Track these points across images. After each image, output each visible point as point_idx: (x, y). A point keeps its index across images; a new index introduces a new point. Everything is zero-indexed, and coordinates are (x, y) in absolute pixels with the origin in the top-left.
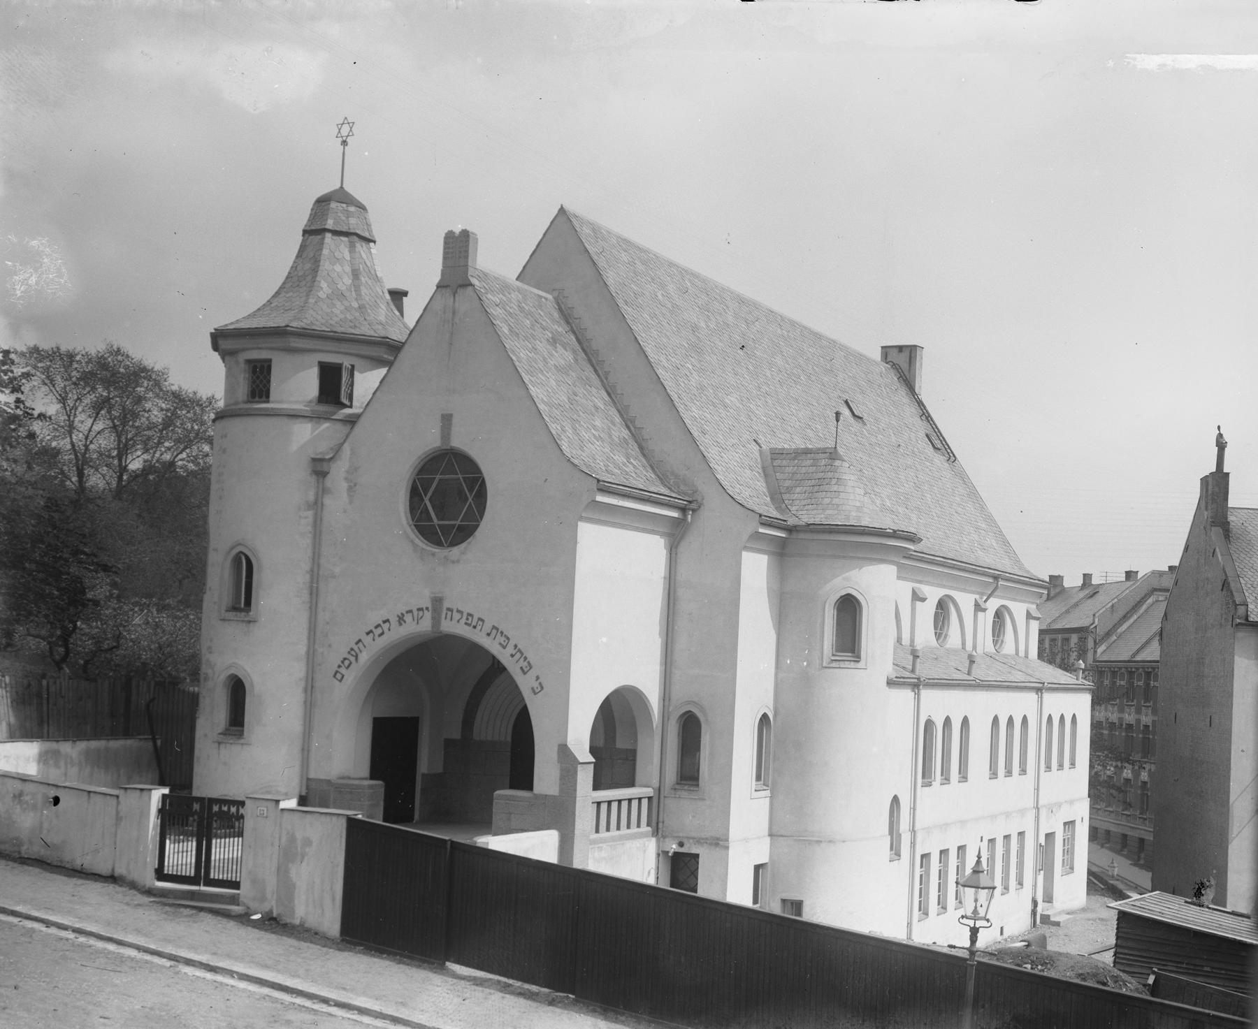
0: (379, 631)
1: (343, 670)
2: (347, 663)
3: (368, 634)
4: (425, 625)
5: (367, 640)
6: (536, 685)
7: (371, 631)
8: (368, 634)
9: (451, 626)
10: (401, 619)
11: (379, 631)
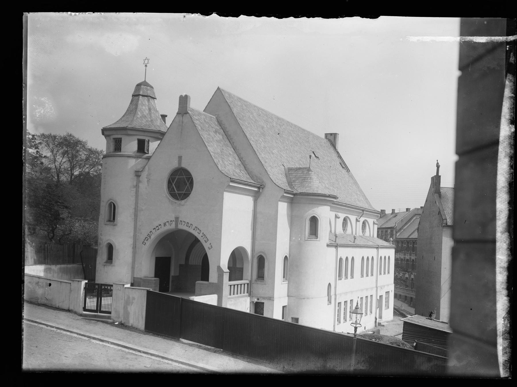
0: (158, 228)
1: (145, 241)
6: (210, 246)
9: (181, 227)
10: (165, 224)
11: (158, 228)
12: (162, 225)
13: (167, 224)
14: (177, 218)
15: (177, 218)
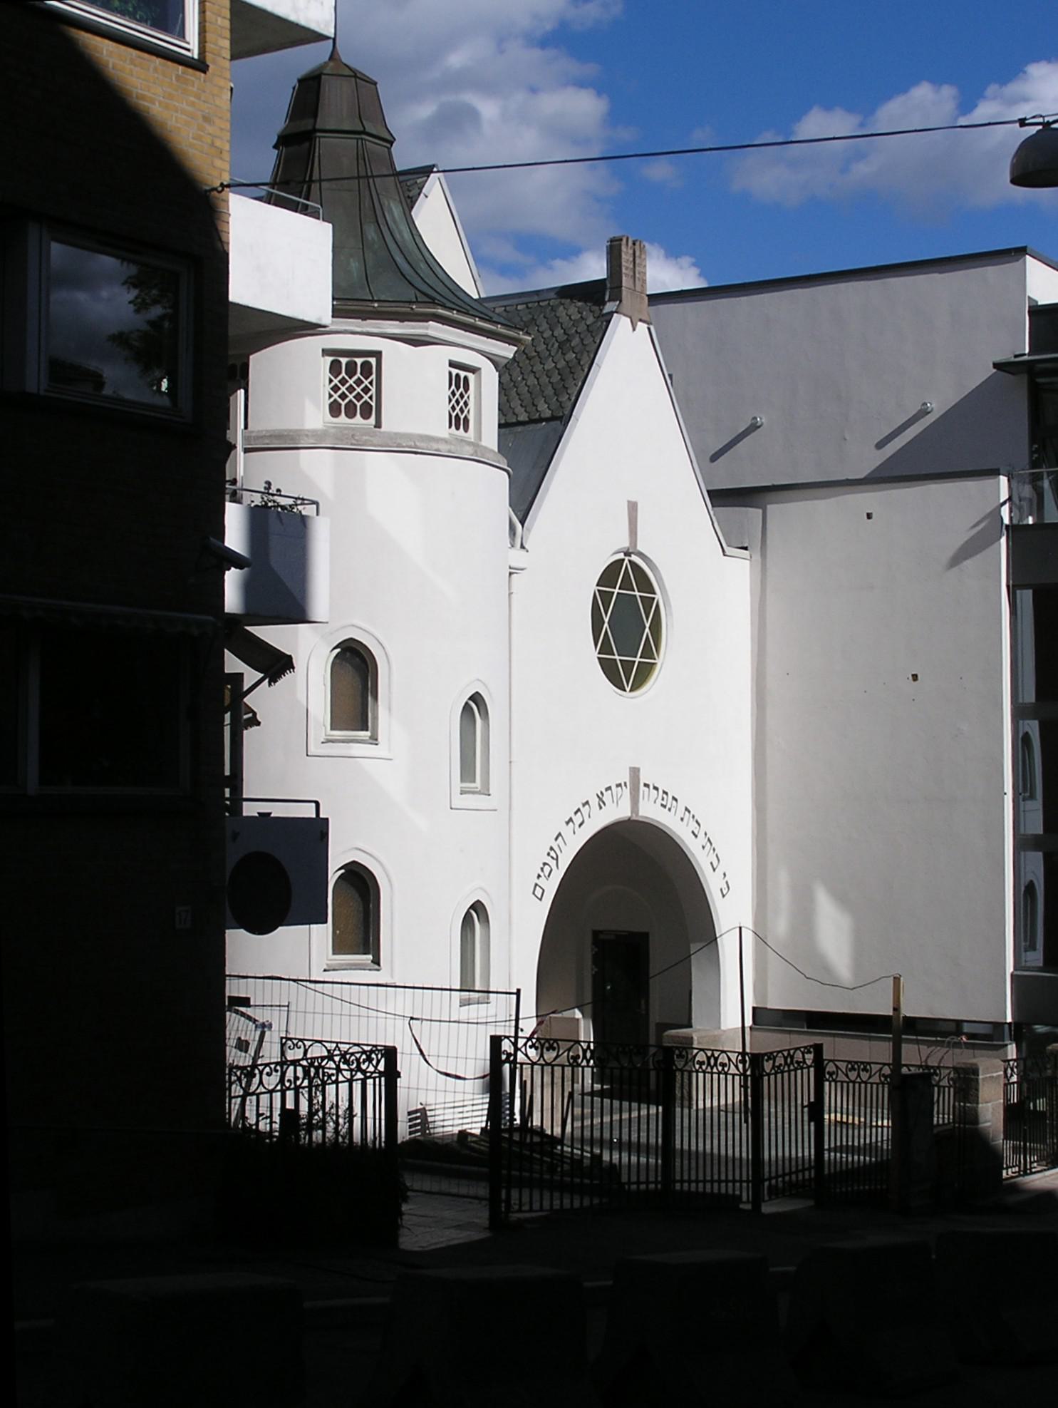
2: (547, 869)
3: (567, 823)
4: (618, 811)
5: (702, 840)
7: (571, 820)
8: (567, 823)
9: (650, 811)
11: (578, 819)
12: (594, 802)
13: (607, 797)
14: (635, 772)
15: (635, 772)
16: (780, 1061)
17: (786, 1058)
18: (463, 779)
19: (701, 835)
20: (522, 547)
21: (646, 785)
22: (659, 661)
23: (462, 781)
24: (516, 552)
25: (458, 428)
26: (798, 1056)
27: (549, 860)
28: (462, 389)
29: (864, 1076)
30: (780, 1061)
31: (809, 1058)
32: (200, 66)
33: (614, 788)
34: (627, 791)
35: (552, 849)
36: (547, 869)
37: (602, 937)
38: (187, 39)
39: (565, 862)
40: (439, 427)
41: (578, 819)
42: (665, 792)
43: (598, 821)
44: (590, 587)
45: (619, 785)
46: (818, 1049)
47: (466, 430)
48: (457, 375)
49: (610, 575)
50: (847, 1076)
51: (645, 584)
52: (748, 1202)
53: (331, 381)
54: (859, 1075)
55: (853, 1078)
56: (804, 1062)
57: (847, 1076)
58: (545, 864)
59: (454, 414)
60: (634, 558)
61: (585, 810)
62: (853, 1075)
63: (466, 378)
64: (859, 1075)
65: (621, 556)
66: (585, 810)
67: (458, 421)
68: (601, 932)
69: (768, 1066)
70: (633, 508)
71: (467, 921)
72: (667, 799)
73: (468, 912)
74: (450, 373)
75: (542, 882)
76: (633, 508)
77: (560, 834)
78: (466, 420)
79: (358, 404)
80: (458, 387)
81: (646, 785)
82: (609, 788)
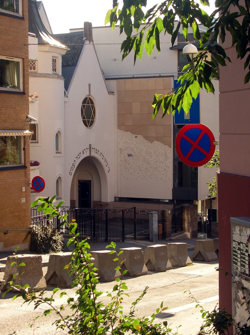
2: (72, 168)
3: (76, 158)
4: (87, 154)
5: (104, 160)
8: (76, 158)
9: (93, 154)
11: (78, 157)
12: (82, 153)
14: (90, 145)
15: (90, 145)
16: (128, 211)
17: (129, 210)
18: (56, 150)
19: (104, 159)
20: (67, 97)
21: (93, 148)
22: (95, 120)
23: (56, 150)
24: (66, 98)
25: (54, 71)
26: (131, 210)
27: (73, 166)
28: (55, 62)
29: (144, 213)
30: (128, 211)
31: (133, 210)
32: (22, 18)
33: (86, 149)
34: (88, 150)
35: (73, 164)
36: (72, 168)
37: (80, 181)
38: (19, 13)
39: (76, 166)
40: (51, 72)
41: (78, 157)
42: (96, 150)
43: (83, 157)
44: (81, 104)
45: (87, 149)
46: (135, 208)
47: (55, 72)
48: (54, 59)
49: (85, 101)
50: (140, 213)
51: (92, 103)
52: (122, 240)
53: (35, 65)
54: (143, 213)
55: (142, 214)
56: (132, 211)
57: (140, 213)
58: (72, 167)
59: (53, 68)
60: (90, 97)
61: (80, 155)
62: (142, 213)
63: (55, 59)
64: (143, 213)
65: (87, 97)
66: (80, 155)
67: (54, 70)
68: (80, 180)
69: (125, 212)
70: (90, 85)
71: (57, 181)
72: (97, 151)
73: (57, 179)
74: (52, 59)
75: (71, 171)
76: (90, 85)
77: (75, 160)
78: (56, 69)
79: (32, 67)
80: (54, 62)
81: (93, 148)
82: (85, 150)
